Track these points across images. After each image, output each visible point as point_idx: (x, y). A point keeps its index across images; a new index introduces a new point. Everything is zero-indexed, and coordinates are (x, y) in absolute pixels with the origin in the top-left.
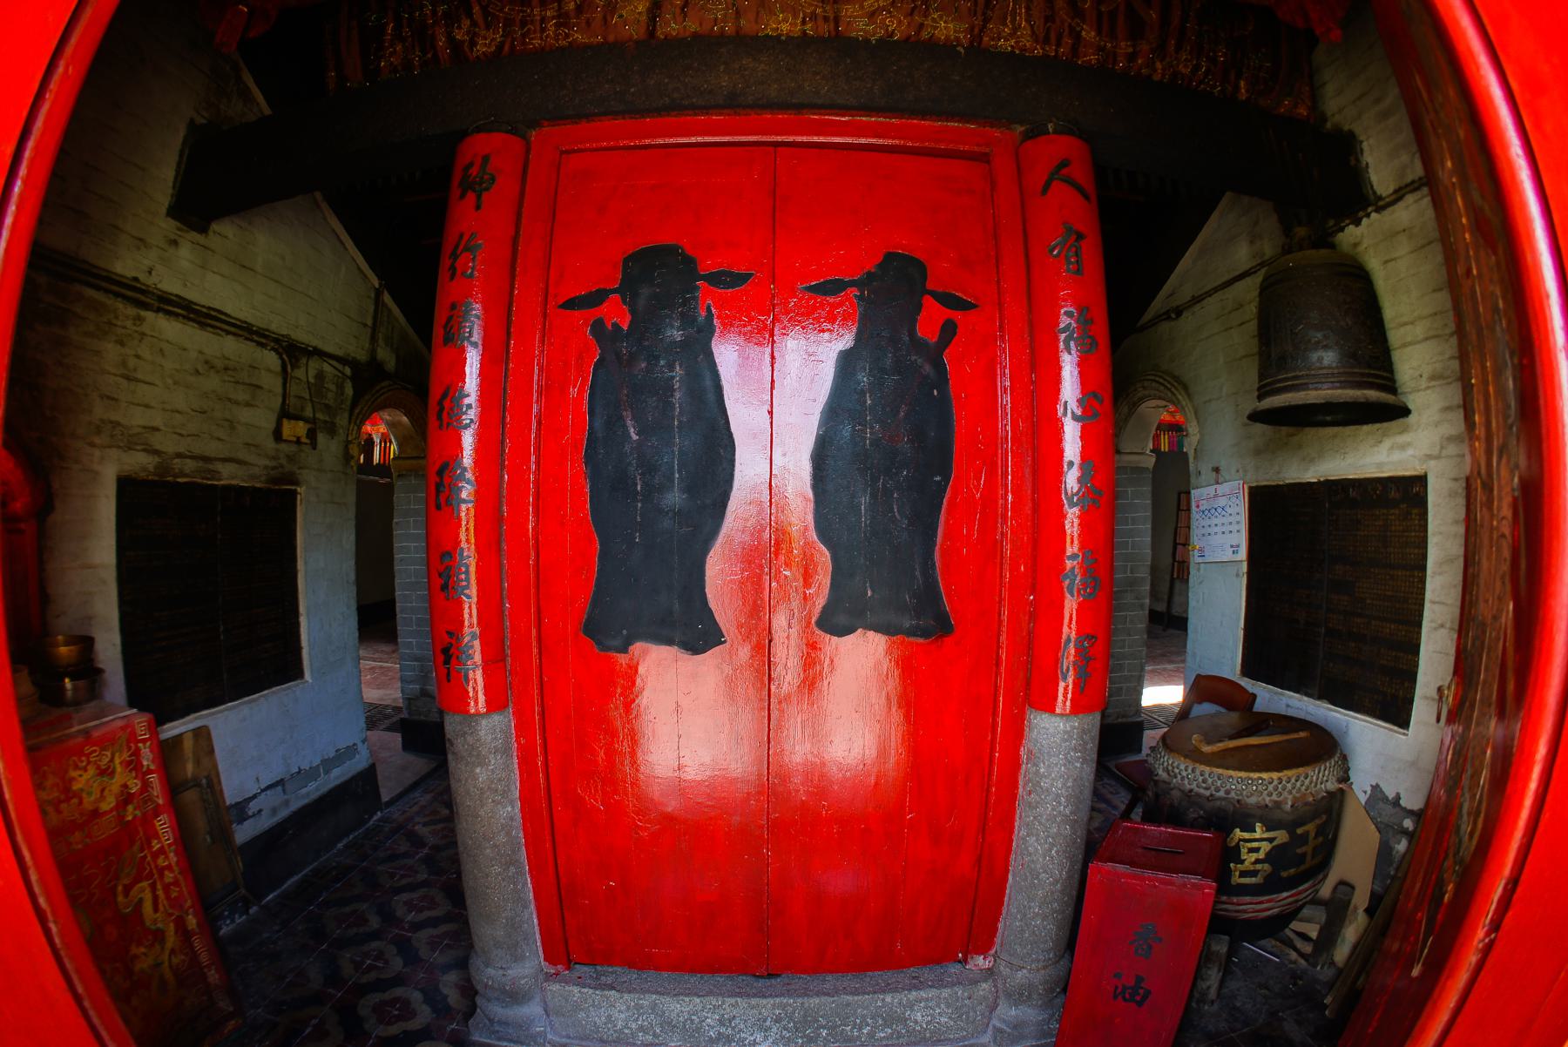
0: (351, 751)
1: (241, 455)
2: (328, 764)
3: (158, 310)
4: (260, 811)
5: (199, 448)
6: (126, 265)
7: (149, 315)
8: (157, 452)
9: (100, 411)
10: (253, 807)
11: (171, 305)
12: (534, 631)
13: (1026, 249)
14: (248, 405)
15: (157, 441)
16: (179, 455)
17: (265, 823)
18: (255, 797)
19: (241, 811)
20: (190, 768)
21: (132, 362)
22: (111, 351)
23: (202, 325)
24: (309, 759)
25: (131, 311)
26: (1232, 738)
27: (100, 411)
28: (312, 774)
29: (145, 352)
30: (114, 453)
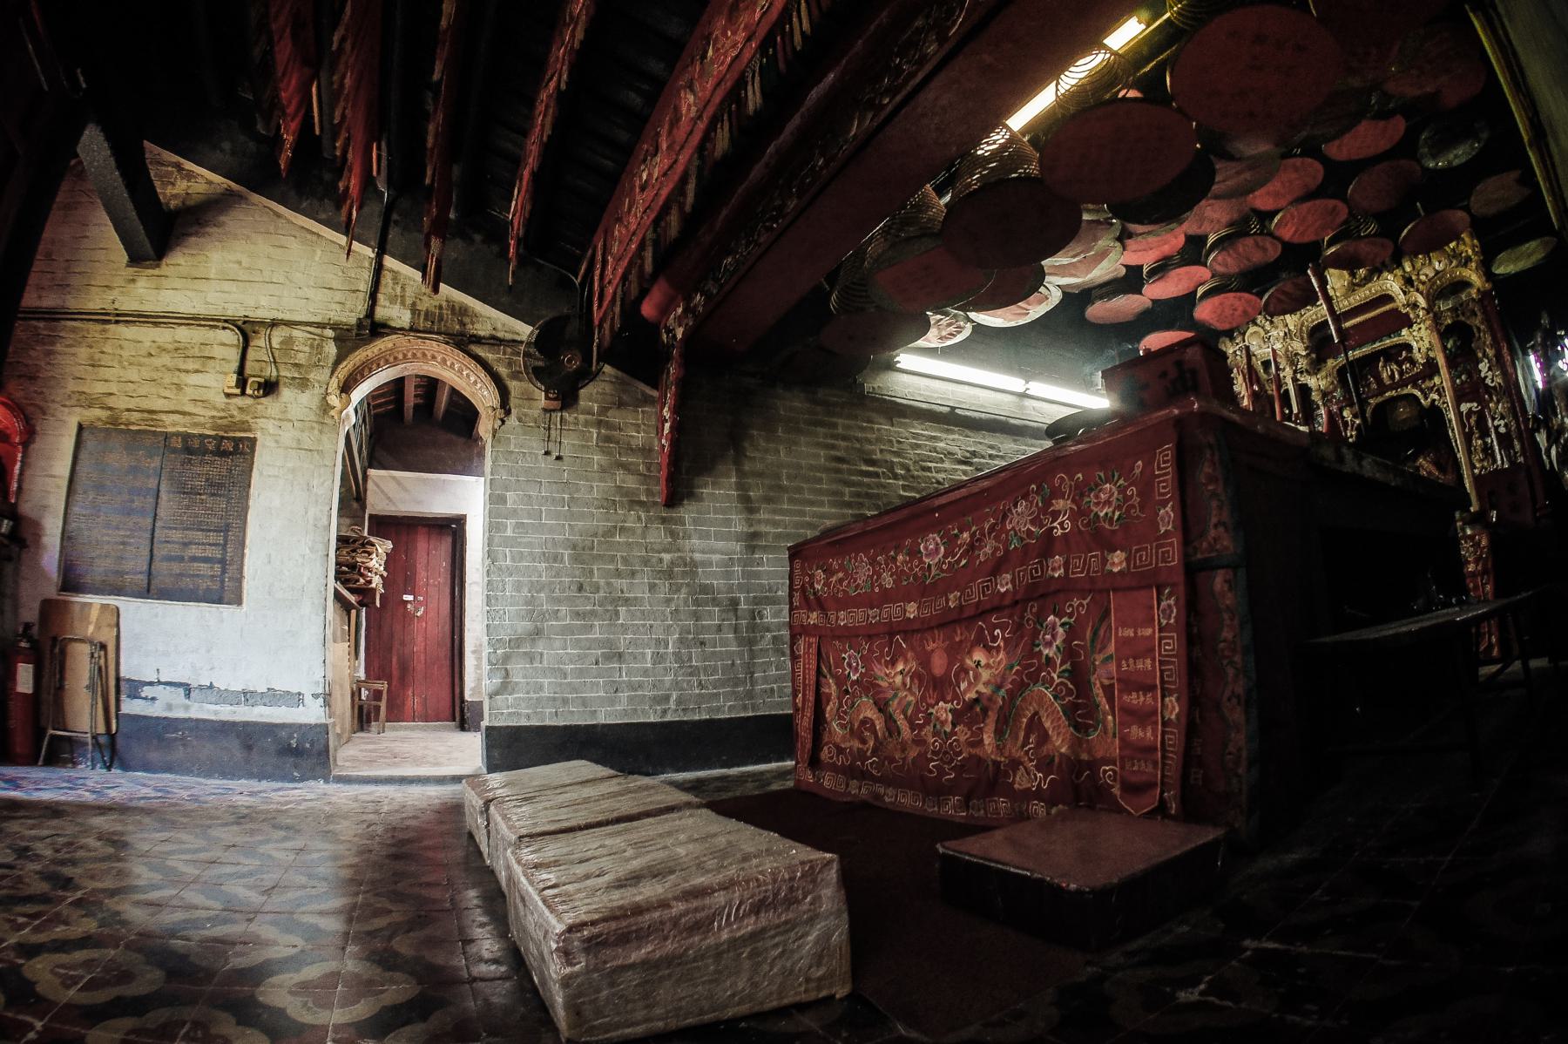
0: (298, 699)
1: (187, 409)
2: (247, 696)
3: (117, 322)
4: (153, 699)
5: (146, 404)
6: (95, 302)
7: (112, 327)
8: (110, 409)
9: (72, 386)
10: (147, 691)
11: (121, 318)
12: (757, 172)
13: (599, 824)
14: (197, 371)
15: (111, 402)
16: (128, 410)
17: (155, 710)
18: (151, 684)
19: (135, 689)
20: (91, 629)
21: (98, 356)
22: (83, 352)
23: (156, 324)
24: (228, 680)
25: (99, 327)
26: (66, 536)
27: (72, 386)
28: (226, 697)
29: (108, 349)
30: (78, 409)
